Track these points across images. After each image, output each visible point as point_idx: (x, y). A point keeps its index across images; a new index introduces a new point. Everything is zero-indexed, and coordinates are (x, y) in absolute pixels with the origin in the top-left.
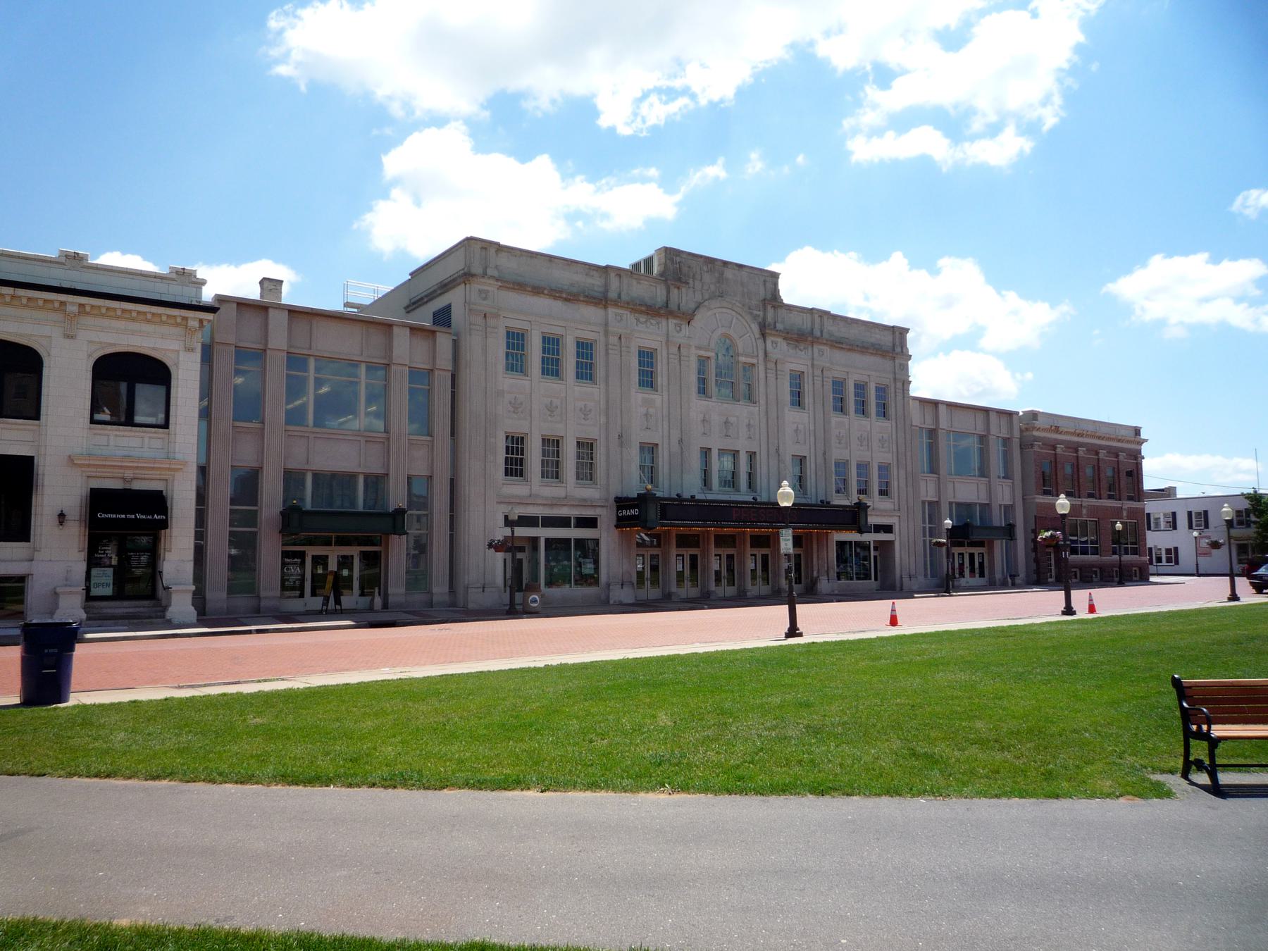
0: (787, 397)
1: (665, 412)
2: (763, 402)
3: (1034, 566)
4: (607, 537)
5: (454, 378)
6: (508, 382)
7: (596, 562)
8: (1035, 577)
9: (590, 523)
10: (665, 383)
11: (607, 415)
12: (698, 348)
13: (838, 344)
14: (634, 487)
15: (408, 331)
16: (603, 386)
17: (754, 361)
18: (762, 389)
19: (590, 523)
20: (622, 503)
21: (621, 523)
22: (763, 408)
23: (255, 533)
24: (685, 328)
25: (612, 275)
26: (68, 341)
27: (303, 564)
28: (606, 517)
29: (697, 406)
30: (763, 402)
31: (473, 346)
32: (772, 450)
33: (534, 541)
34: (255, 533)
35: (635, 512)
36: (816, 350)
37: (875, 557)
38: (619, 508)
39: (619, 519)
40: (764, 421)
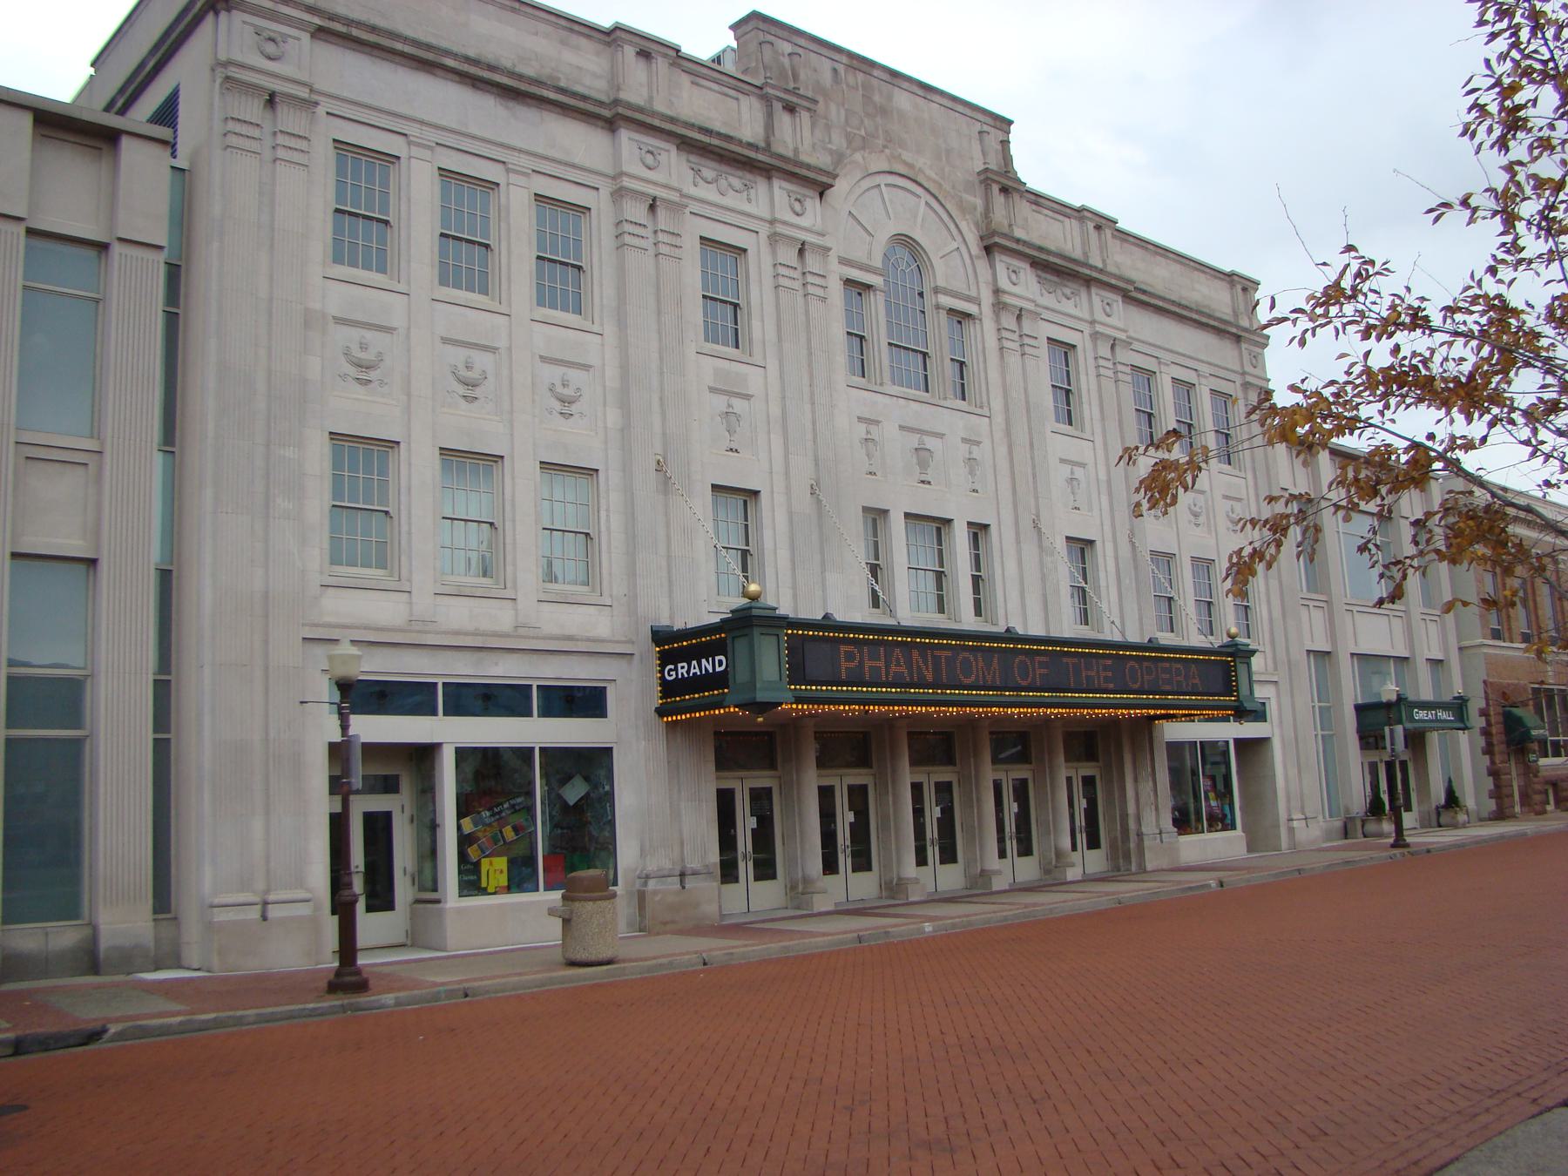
0: (1047, 400)
1: (775, 410)
2: (997, 404)
3: (1489, 783)
4: (629, 732)
5: (174, 274)
6: (338, 292)
7: (459, 828)
8: (1491, 805)
9: (584, 701)
10: (771, 335)
11: (625, 405)
12: (844, 261)
13: (1135, 296)
14: (704, 605)
15: (27, 120)
16: (610, 330)
17: (972, 308)
18: (994, 375)
19: (584, 701)
20: (672, 645)
21: (674, 697)
22: (999, 419)
23: (78, 743)
24: (812, 204)
25: (630, 51)
26: (654, 465)
27: (427, 790)
28: (633, 692)
29: (849, 402)
30: (997, 404)
31: (232, 184)
32: (1026, 523)
33: (424, 755)
34: (78, 743)
35: (700, 671)
36: (1096, 300)
37: (239, 1021)
38: (666, 658)
39: (668, 689)
40: (1002, 450)
